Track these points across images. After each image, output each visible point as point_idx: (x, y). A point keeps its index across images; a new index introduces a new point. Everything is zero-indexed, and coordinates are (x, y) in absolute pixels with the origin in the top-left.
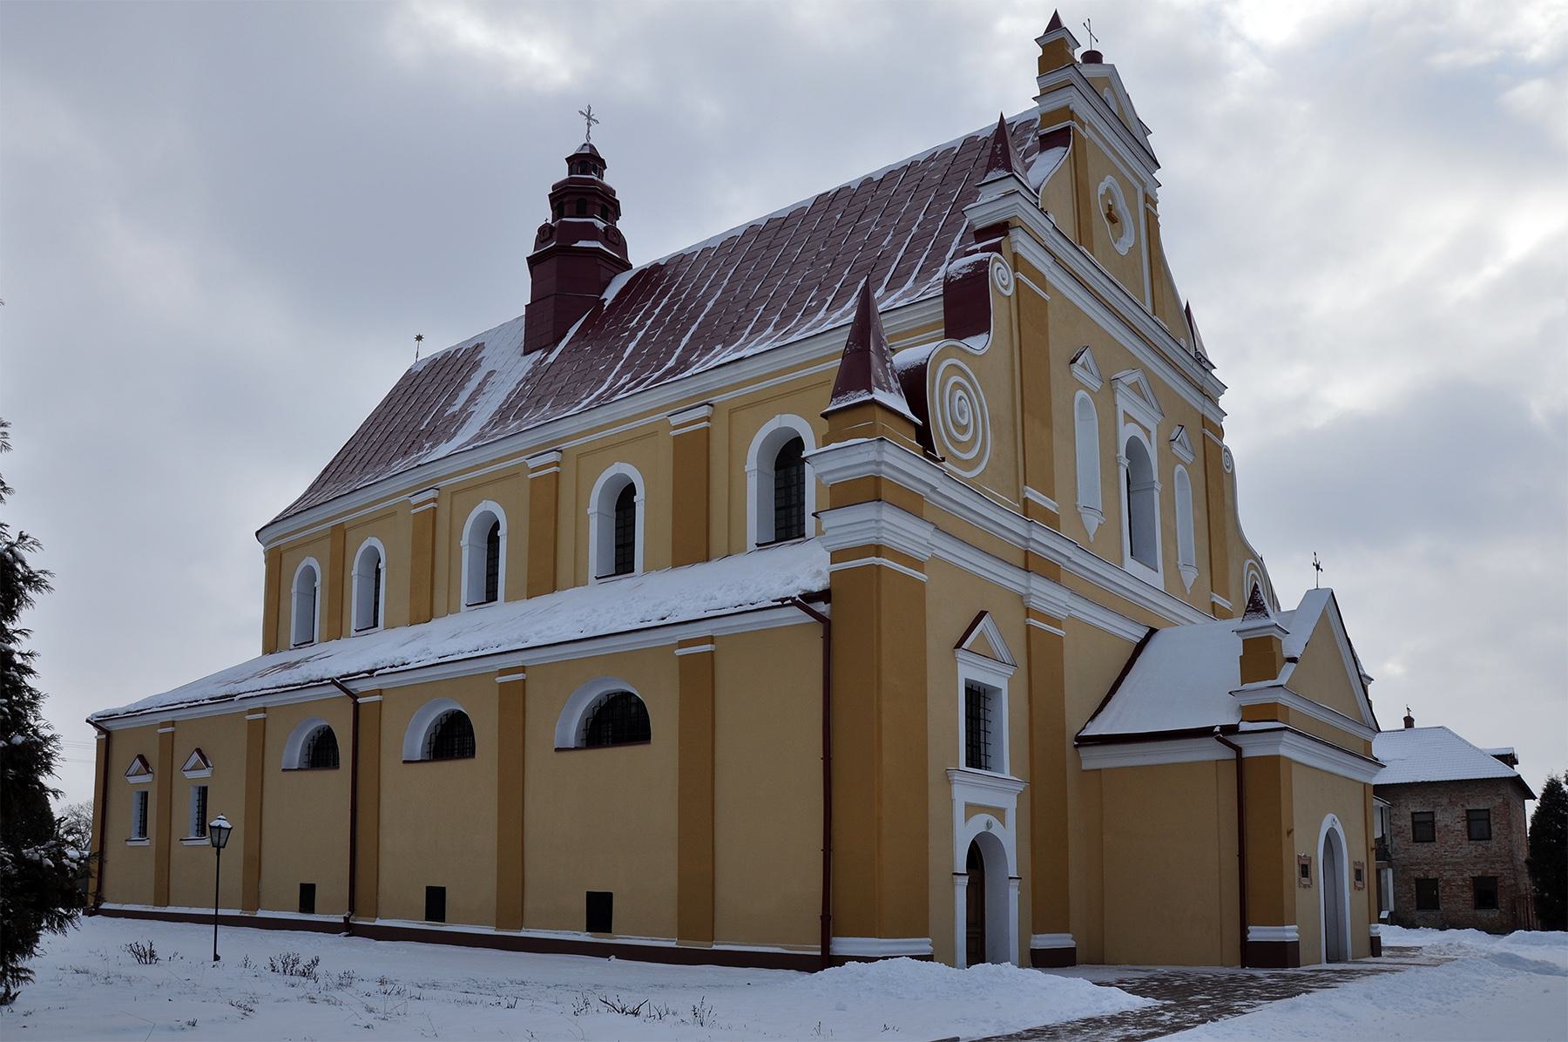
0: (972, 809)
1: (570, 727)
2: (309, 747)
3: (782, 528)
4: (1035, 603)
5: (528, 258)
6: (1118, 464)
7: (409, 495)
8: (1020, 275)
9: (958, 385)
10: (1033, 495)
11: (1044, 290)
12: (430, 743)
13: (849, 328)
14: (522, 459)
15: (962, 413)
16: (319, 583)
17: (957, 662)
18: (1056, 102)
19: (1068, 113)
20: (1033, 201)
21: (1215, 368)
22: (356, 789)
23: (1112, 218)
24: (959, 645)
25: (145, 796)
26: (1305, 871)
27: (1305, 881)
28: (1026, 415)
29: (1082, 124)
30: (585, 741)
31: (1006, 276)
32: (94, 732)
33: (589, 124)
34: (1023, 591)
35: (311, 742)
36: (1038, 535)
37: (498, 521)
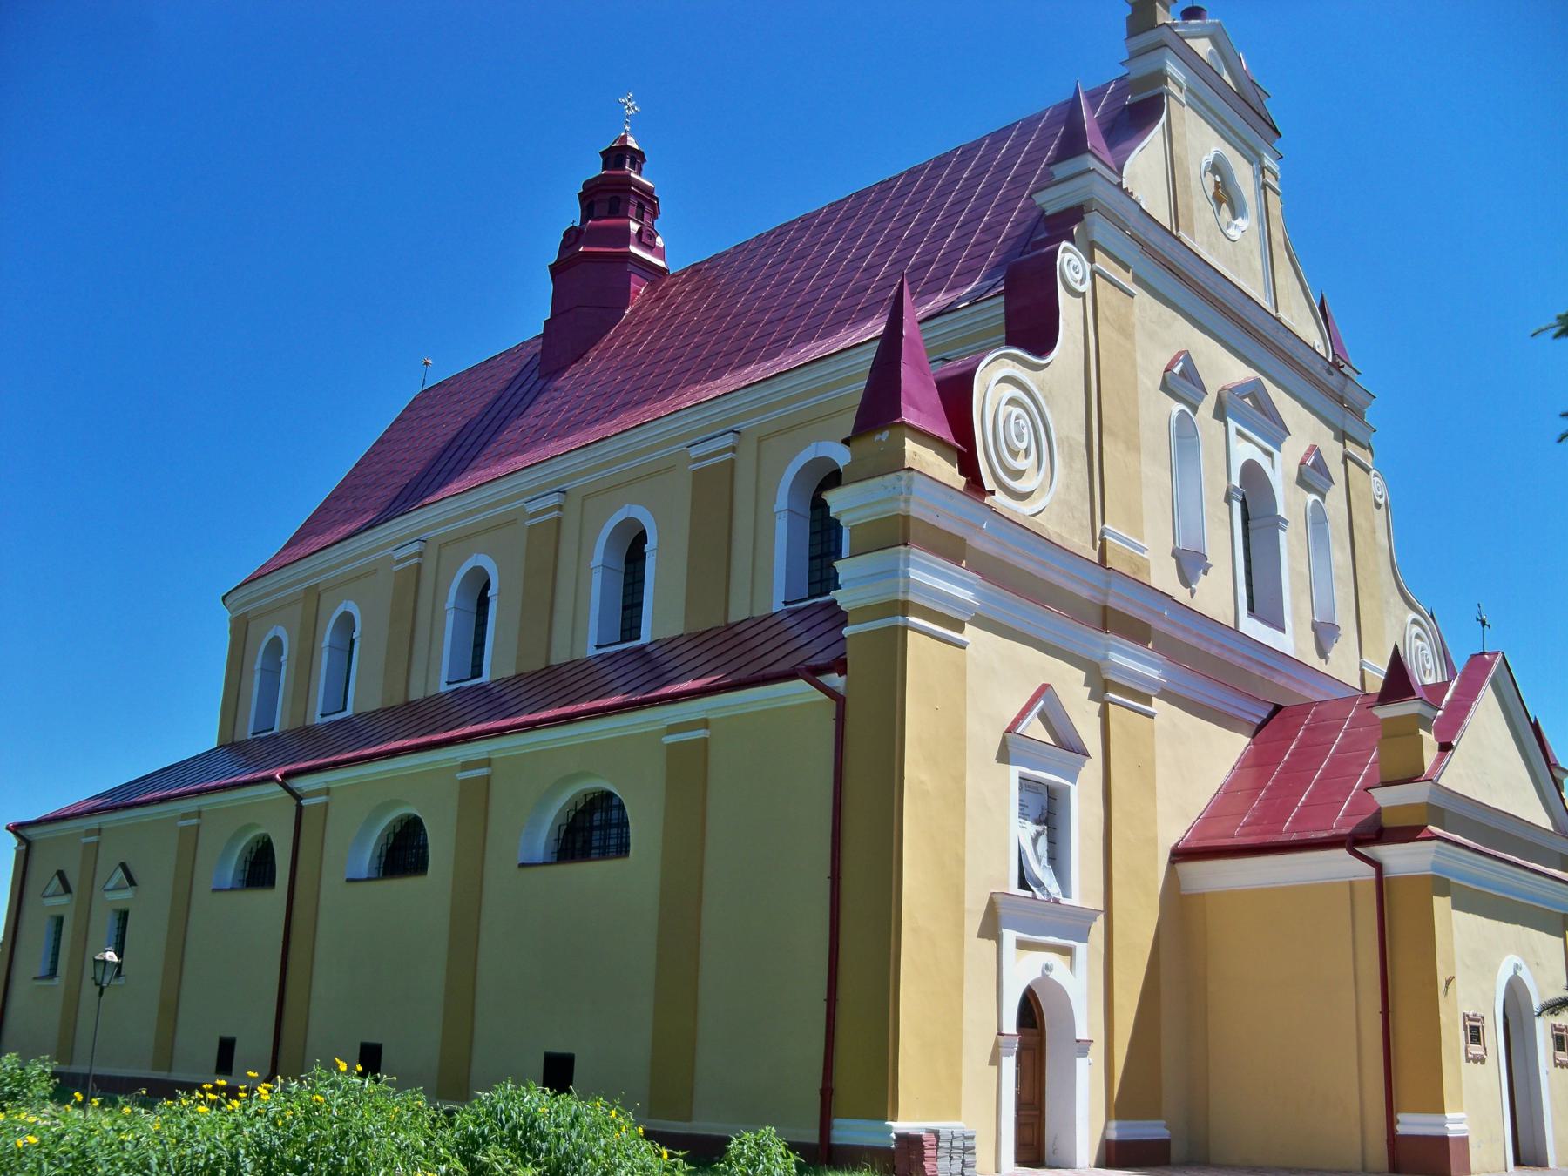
1: (541, 839)
2: (245, 861)
3: (816, 582)
5: (549, 266)
7: (526, 499)
12: (380, 857)
13: (877, 343)
14: (386, 552)
15: (1020, 437)
16: (496, 592)
22: (291, 914)
25: (59, 921)
26: (1475, 1035)
27: (1476, 1050)
30: (555, 855)
31: (1080, 268)
32: (14, 841)
35: (248, 856)
37: (644, 531)
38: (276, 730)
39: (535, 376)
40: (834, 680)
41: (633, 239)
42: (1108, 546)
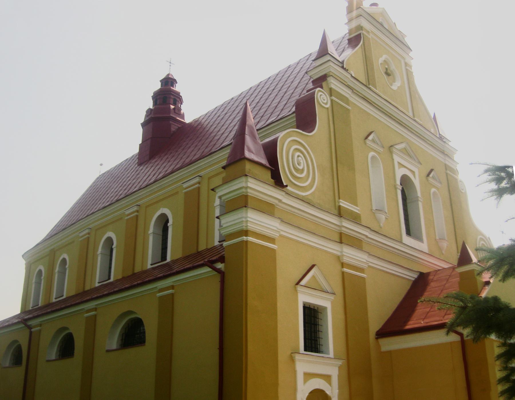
0: (308, 376)
4: (345, 260)
6: (396, 188)
8: (333, 98)
9: (297, 150)
10: (344, 204)
11: (348, 105)
15: (299, 164)
17: (297, 292)
18: (354, 24)
19: (360, 28)
20: (341, 65)
21: (450, 141)
23: (388, 74)
24: (298, 283)
28: (339, 165)
29: (368, 32)
31: (325, 98)
33: (170, 66)
34: (339, 254)
36: (346, 224)
38: (40, 305)
39: (136, 165)
40: (220, 266)
41: (172, 111)
42: (341, 208)
